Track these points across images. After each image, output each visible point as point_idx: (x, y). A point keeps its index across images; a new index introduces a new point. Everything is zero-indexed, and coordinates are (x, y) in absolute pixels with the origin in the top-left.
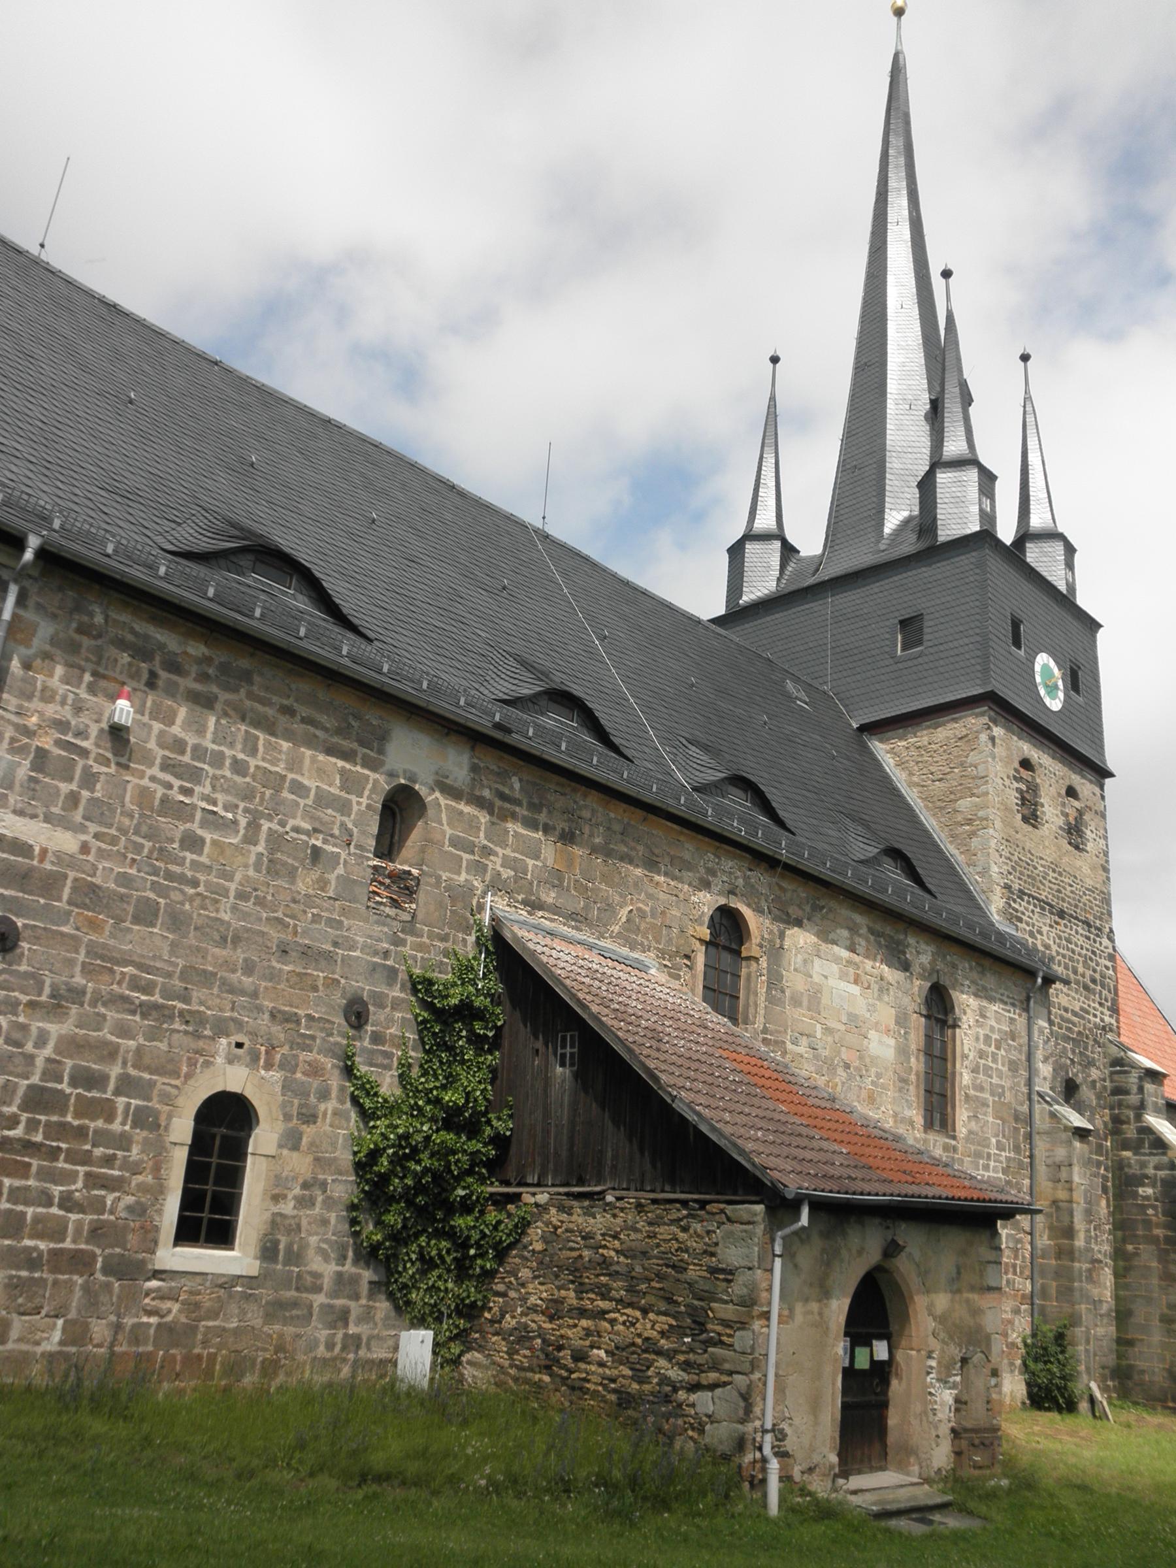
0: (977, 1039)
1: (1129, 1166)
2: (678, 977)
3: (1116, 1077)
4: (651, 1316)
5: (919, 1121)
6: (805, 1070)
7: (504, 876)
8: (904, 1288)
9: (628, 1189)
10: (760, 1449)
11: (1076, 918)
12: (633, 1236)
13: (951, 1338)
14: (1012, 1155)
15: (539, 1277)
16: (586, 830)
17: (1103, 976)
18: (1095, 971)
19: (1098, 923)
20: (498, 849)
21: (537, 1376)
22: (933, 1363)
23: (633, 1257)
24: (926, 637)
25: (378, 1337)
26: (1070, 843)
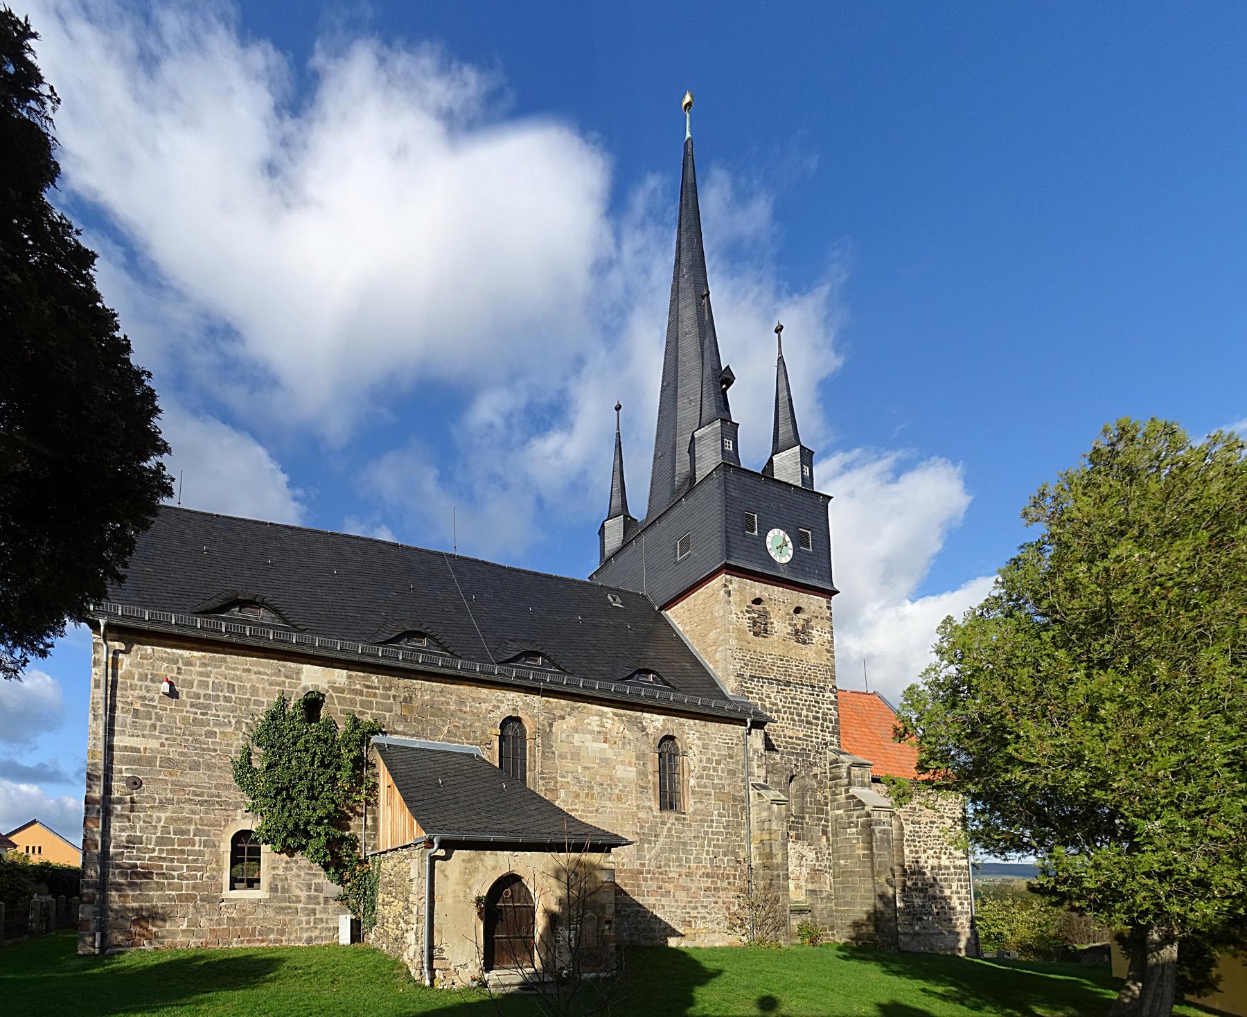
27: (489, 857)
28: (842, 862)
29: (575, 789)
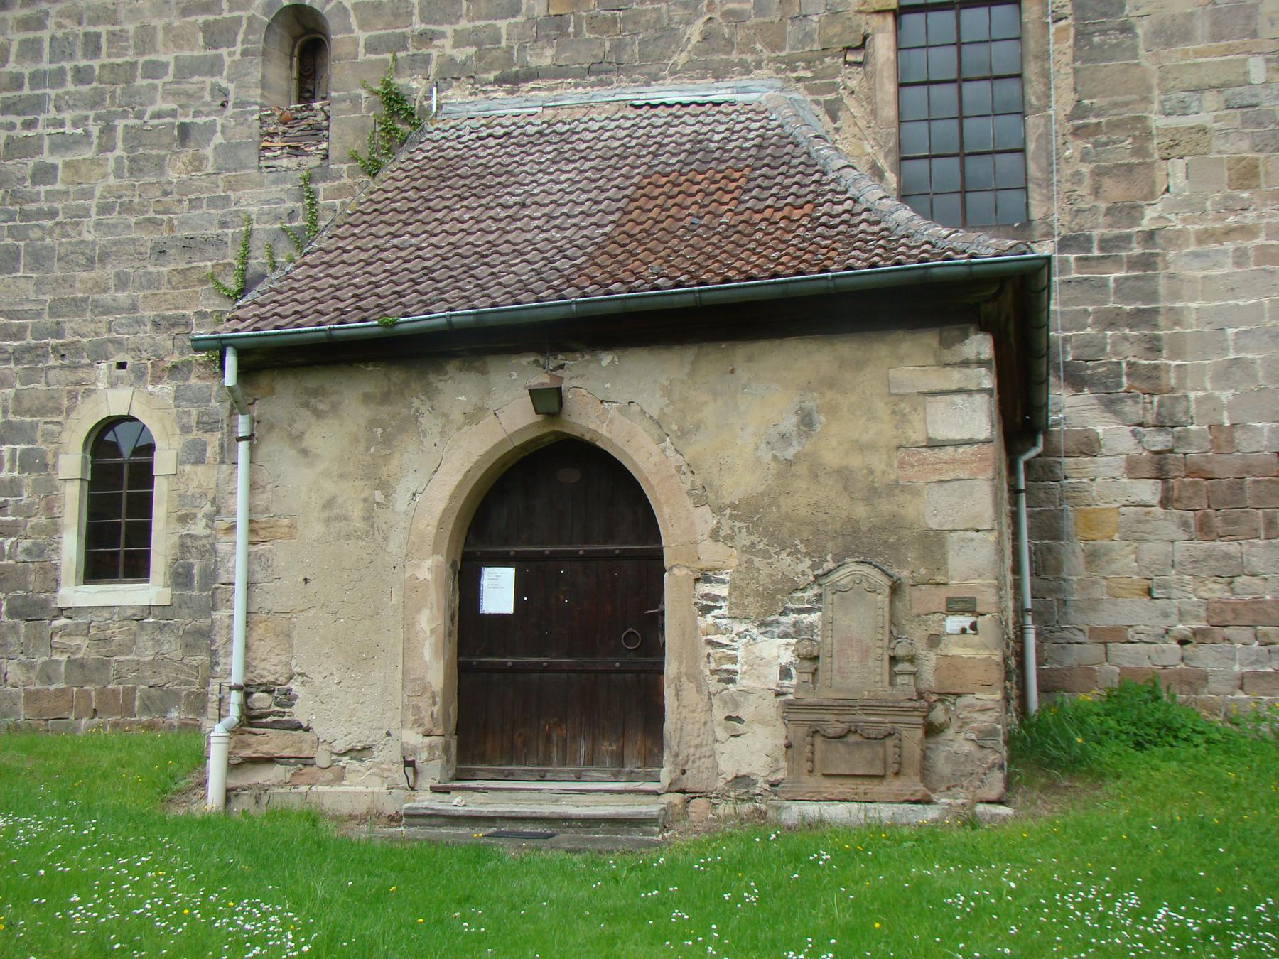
27: (457, 390)
29: (1241, 147)
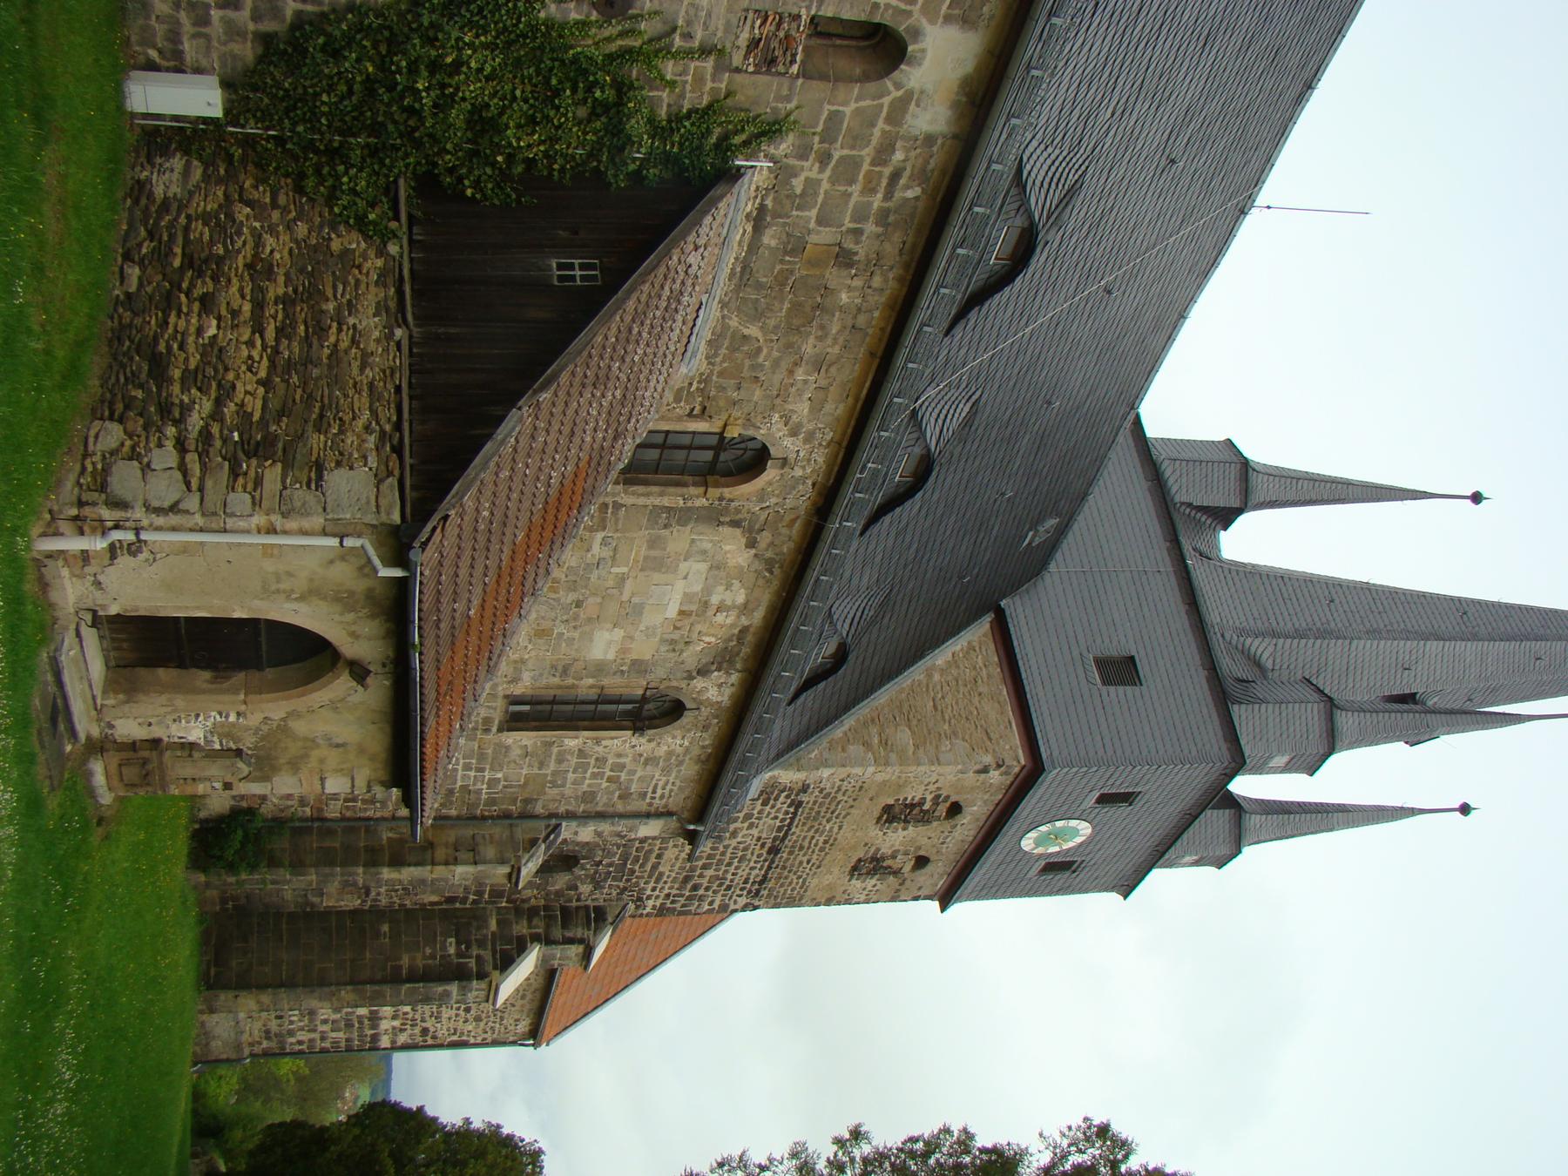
0: (619, 755)
1: (479, 928)
2: (678, 399)
3: (582, 913)
4: (261, 390)
5: (518, 690)
6: (571, 556)
7: (794, 182)
8: (316, 684)
9: (411, 354)
10: (116, 527)
11: (769, 868)
12: (356, 365)
13: (263, 738)
14: (484, 796)
15: (299, 248)
16: (857, 283)
17: (701, 898)
18: (707, 889)
19: (765, 893)
20: (828, 172)
21: (178, 250)
22: (232, 718)
23: (330, 367)
24: (1112, 689)
25: (208, 48)
26: (860, 860)
28: (385, 928)
